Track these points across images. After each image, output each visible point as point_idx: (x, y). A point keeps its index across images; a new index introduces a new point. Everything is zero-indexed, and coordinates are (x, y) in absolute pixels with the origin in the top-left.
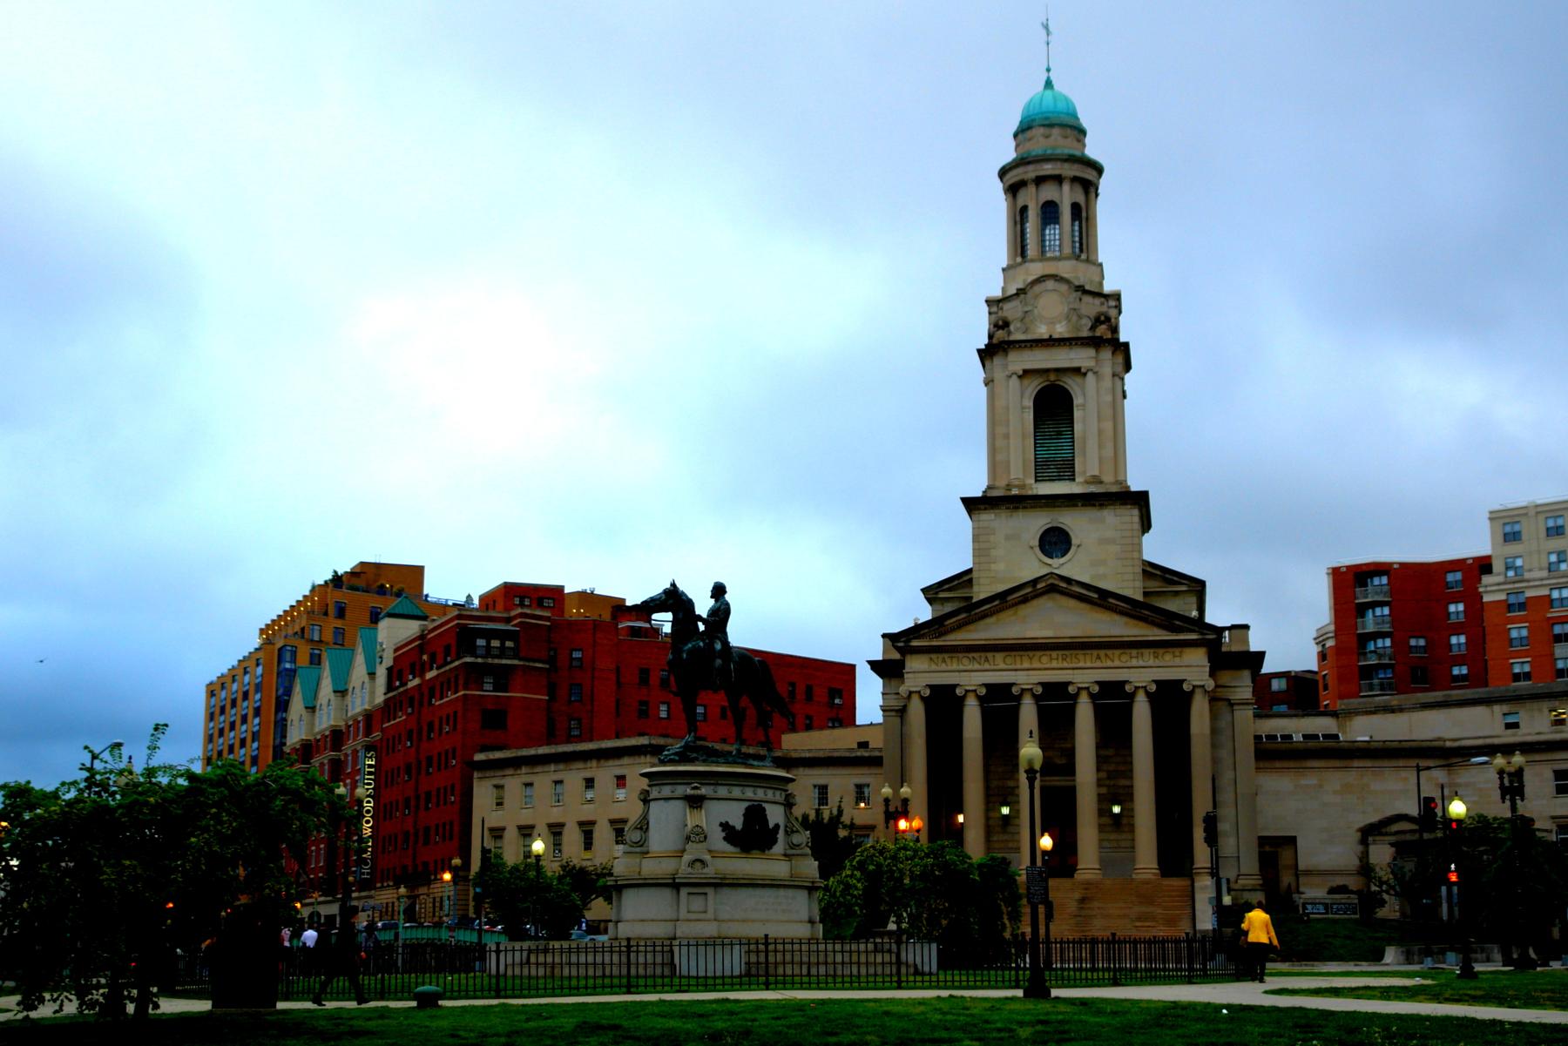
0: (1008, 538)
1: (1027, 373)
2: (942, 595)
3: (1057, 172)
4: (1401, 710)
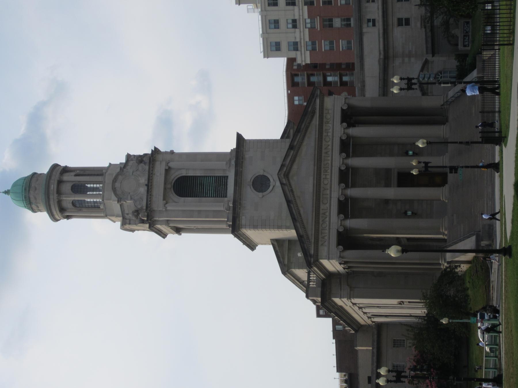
2: (286, 262)
3: (56, 183)
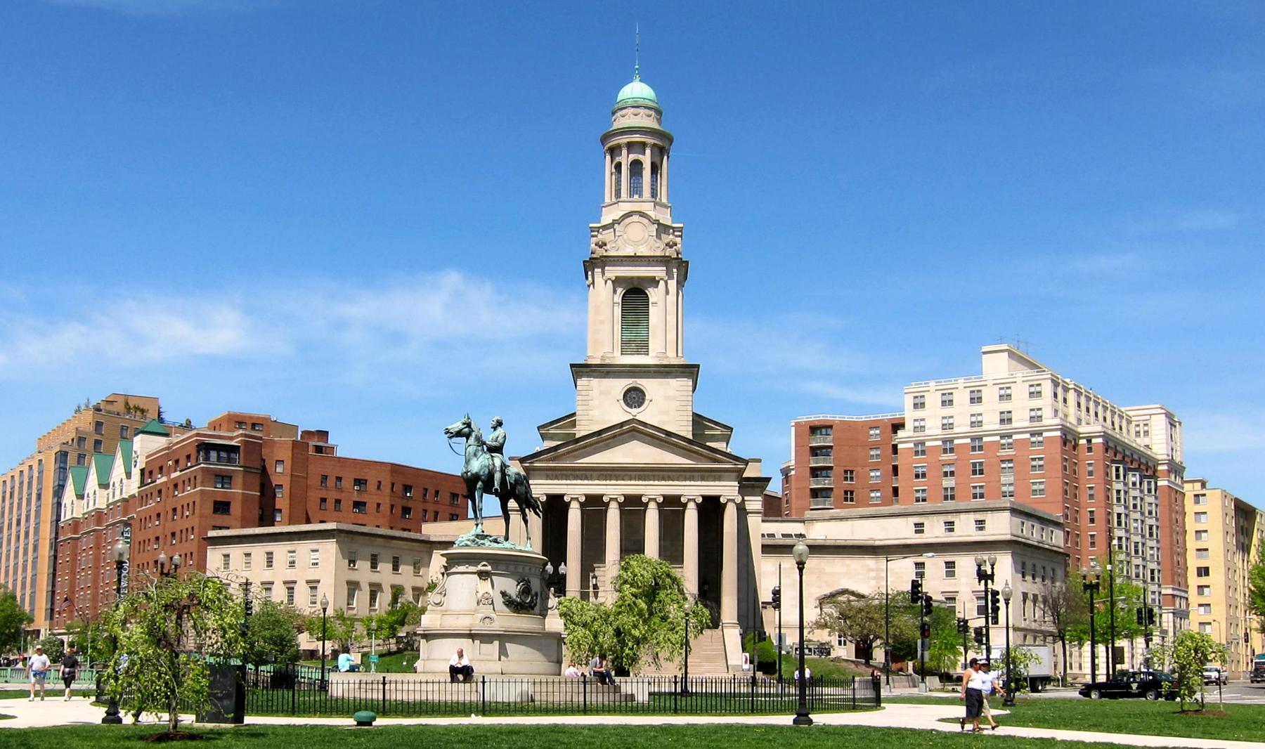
0: (601, 393)
1: (617, 282)
4: (847, 519)
